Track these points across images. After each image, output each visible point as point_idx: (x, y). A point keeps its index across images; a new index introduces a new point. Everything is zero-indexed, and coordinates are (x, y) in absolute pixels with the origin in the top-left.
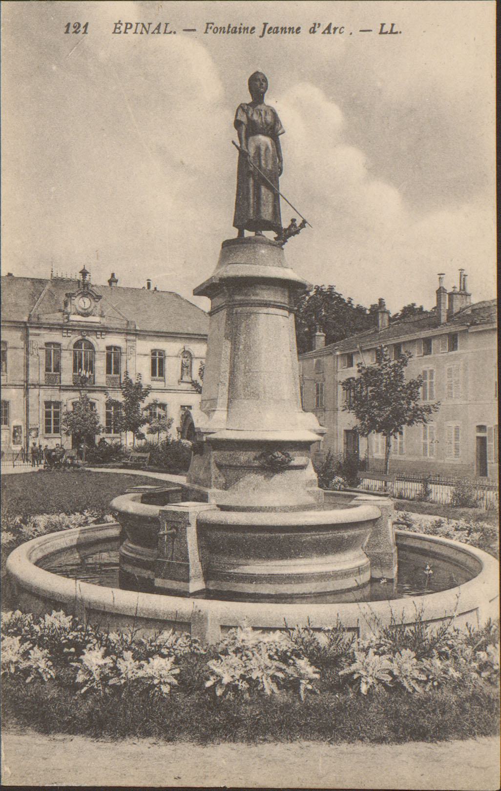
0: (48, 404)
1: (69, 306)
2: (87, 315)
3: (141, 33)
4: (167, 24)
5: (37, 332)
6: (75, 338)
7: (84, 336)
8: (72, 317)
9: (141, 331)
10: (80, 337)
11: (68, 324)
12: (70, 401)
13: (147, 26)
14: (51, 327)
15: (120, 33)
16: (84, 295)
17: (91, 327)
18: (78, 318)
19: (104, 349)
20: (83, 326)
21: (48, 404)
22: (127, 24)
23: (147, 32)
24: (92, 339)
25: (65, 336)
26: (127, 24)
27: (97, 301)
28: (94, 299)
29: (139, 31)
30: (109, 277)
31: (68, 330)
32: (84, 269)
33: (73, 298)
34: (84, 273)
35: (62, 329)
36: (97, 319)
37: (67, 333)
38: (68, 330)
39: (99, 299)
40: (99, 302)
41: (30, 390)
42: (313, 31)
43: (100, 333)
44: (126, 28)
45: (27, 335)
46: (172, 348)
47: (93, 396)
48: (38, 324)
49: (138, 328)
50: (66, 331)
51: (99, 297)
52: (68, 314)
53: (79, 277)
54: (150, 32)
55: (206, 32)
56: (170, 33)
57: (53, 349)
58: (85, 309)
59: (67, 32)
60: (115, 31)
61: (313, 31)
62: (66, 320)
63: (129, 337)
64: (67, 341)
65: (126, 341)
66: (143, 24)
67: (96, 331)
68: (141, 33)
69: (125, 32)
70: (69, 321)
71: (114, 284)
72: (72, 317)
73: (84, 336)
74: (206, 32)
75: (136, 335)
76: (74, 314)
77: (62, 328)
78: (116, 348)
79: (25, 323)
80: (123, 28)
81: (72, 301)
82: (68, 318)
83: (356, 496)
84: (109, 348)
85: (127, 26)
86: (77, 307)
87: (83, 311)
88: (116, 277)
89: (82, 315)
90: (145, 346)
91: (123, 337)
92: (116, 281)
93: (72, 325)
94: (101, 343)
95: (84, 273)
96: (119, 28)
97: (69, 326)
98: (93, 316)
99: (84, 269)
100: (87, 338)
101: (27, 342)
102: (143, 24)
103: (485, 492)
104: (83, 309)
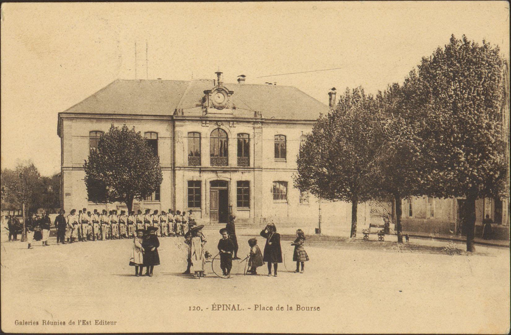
0: (191, 183)
1: (207, 102)
3: (226, 310)
4: (238, 305)
5: (181, 123)
6: (213, 126)
7: (220, 126)
9: (265, 119)
11: (206, 116)
13: (229, 306)
14: (193, 120)
15: (216, 310)
18: (214, 110)
21: (191, 183)
23: (229, 309)
25: (204, 126)
26: (218, 305)
27: (230, 96)
28: (227, 94)
29: (225, 309)
31: (206, 121)
33: (210, 94)
35: (202, 121)
36: (230, 111)
37: (206, 123)
38: (206, 121)
39: (231, 94)
40: (231, 97)
41: (176, 171)
43: (232, 123)
44: (218, 308)
45: (174, 127)
48: (183, 117)
49: (263, 117)
50: (204, 122)
51: (231, 93)
53: (215, 77)
54: (231, 309)
55: (255, 310)
56: (241, 310)
57: (195, 136)
58: (220, 104)
59: (190, 310)
63: (256, 126)
64: (206, 130)
65: (254, 128)
67: (229, 121)
68: (226, 310)
69: (218, 310)
73: (220, 126)
74: (255, 310)
75: (262, 123)
76: (211, 108)
77: (203, 120)
79: (172, 116)
80: (217, 308)
81: (209, 97)
82: (206, 111)
89: (218, 108)
91: (251, 125)
96: (215, 307)
97: (207, 117)
98: (227, 108)
100: (222, 127)
101: (174, 133)
102: (226, 305)
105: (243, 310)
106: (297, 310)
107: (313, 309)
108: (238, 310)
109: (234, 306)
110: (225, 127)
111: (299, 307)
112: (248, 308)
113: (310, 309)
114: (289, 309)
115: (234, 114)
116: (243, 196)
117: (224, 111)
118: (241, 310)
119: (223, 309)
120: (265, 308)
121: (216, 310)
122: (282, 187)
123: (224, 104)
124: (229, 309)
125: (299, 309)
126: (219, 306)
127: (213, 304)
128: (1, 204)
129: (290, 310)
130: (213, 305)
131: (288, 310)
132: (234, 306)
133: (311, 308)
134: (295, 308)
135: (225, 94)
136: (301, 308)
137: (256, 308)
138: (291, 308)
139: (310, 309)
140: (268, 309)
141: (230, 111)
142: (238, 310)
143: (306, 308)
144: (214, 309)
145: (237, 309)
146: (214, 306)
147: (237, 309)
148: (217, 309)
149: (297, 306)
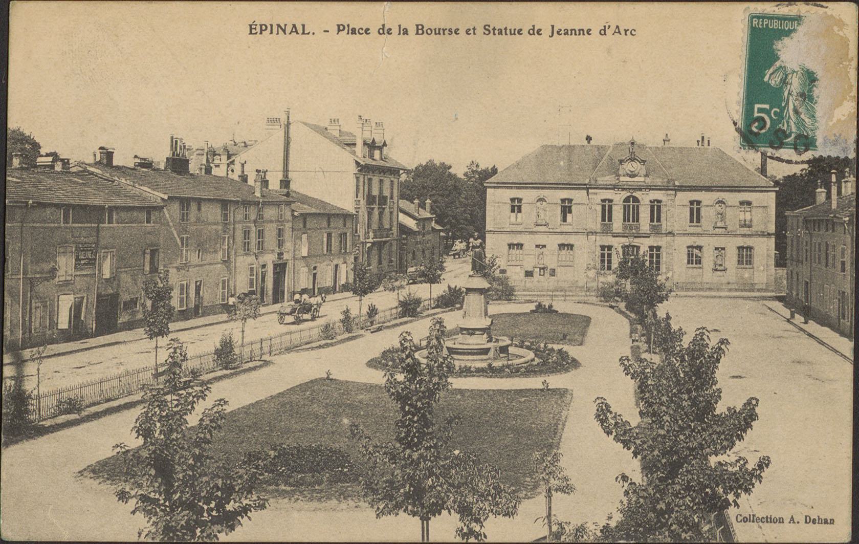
2: (634, 176)
6: (625, 194)
8: (622, 179)
10: (629, 194)
16: (632, 160)
18: (628, 179)
22: (261, 26)
24: (637, 194)
26: (261, 26)
36: (642, 179)
38: (618, 189)
42: (603, 32)
46: (706, 198)
47: (636, 242)
56: (308, 34)
58: (632, 172)
61: (603, 32)
66: (285, 34)
76: (624, 176)
80: (258, 30)
82: (618, 179)
89: (630, 176)
90: (685, 197)
92: (669, 141)
94: (645, 198)
96: (255, 29)
100: (634, 194)
105: (313, 34)
106: (417, 33)
107: (447, 32)
108: (303, 33)
109: (294, 26)
110: (637, 194)
111: (422, 29)
112: (328, 31)
113: (441, 32)
114: (402, 32)
115: (646, 181)
116: (607, 206)
117: (636, 179)
118: (308, 34)
119: (270, 32)
121: (256, 33)
122: (696, 251)
123: (636, 172)
124: (284, 31)
125: (420, 32)
126: (264, 27)
127: (251, 23)
128: (596, 542)
129: (404, 34)
130: (251, 26)
131: (399, 34)
132: (294, 26)
133: (444, 30)
134: (412, 30)
135: (638, 163)
137: (615, 32)
138: (406, 32)
139: (441, 32)
140: (361, 31)
141: (642, 179)
142: (303, 33)
143: (434, 31)
144: (254, 31)
145: (300, 31)
146: (253, 27)
147: (300, 31)
148: (259, 32)
149: (417, 28)
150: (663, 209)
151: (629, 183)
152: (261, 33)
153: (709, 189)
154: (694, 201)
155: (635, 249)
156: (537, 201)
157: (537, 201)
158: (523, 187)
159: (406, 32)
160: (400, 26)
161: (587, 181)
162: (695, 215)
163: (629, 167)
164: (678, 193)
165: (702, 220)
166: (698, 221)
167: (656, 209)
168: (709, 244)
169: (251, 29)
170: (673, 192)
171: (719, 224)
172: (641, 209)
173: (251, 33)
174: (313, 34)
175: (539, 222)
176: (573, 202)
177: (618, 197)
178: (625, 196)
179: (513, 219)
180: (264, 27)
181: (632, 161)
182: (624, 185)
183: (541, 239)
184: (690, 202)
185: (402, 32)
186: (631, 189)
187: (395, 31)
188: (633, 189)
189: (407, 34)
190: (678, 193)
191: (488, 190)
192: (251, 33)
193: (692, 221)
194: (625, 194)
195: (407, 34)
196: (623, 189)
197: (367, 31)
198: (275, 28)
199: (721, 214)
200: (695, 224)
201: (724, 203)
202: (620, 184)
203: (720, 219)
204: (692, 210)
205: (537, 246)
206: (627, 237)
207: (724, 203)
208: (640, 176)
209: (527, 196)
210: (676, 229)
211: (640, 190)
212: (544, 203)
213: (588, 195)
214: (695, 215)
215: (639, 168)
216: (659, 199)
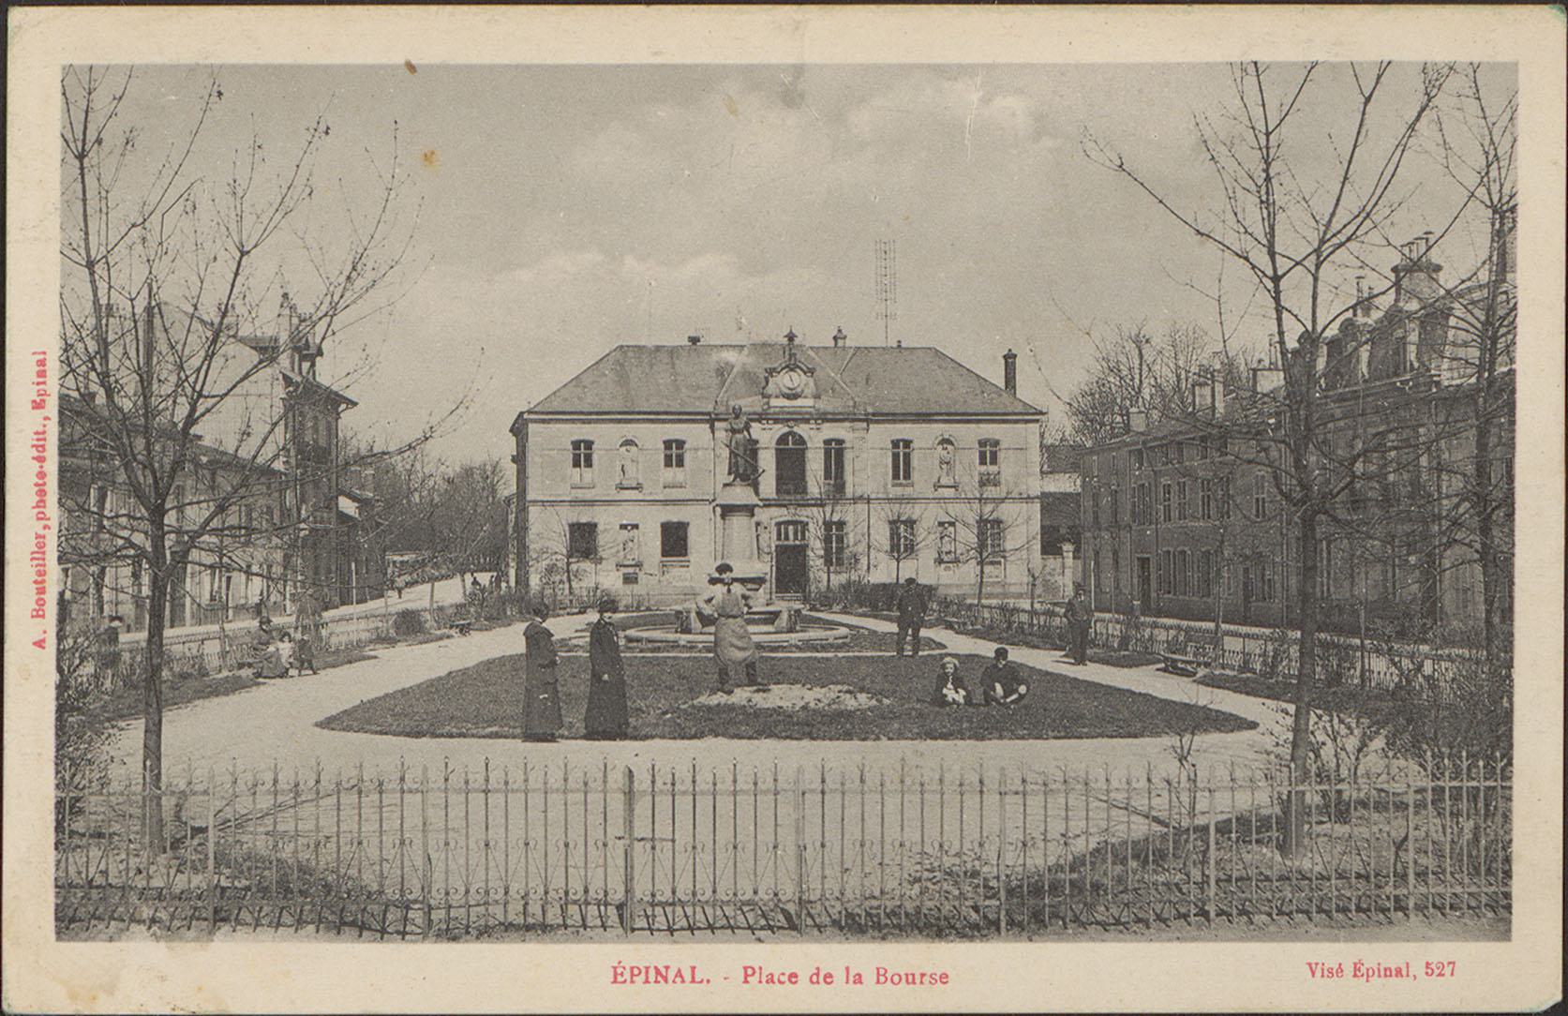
2: (795, 397)
6: (781, 429)
8: (774, 402)
10: (786, 430)
12: (773, 522)
13: (663, 971)
16: (791, 368)
17: (799, 413)
19: (822, 445)
20: (789, 413)
22: (632, 968)
23: (666, 981)
24: (802, 430)
26: (632, 968)
28: (805, 373)
29: (652, 979)
30: (835, 333)
32: (791, 332)
34: (791, 337)
36: (810, 402)
44: (632, 975)
46: (922, 435)
47: (803, 514)
52: (769, 397)
54: (670, 979)
56: (701, 982)
60: (615, 978)
62: (766, 407)
66: (656, 968)
68: (656, 982)
69: (632, 982)
70: (769, 408)
71: (840, 343)
72: (774, 402)
76: (777, 397)
78: (840, 442)
80: (627, 975)
82: (768, 403)
83: (1065, 656)
84: (827, 442)
85: (632, 971)
86: (781, 386)
87: (789, 392)
88: (844, 332)
89: (788, 397)
90: (882, 435)
93: (774, 413)
94: (816, 437)
95: (791, 337)
96: (622, 974)
99: (791, 332)
100: (795, 429)
103: (1187, 738)
104: (789, 389)
106: (878, 982)
108: (693, 981)
110: (802, 430)
114: (851, 979)
117: (799, 402)
118: (701, 982)
120: (904, 980)
121: (625, 981)
123: (799, 390)
127: (616, 964)
129: (855, 982)
136: (889, 975)
137: (746, 975)
138: (859, 979)
142: (693, 981)
144: (620, 979)
146: (619, 971)
148: (629, 980)
150: (848, 456)
151: (786, 409)
152: (632, 982)
153: (924, 417)
154: (898, 441)
155: (791, 528)
156: (621, 446)
157: (621, 446)
158: (603, 420)
159: (859, 979)
160: (847, 969)
161: (710, 408)
162: (902, 465)
163: (786, 380)
164: (871, 426)
165: (915, 475)
166: (907, 476)
167: (835, 452)
168: (928, 516)
169: (616, 974)
170: (865, 425)
171: (944, 481)
172: (809, 454)
173: (615, 981)
174: (708, 981)
175: (626, 483)
176: (686, 446)
177: (766, 436)
178: (780, 433)
179: (576, 478)
180: (636, 972)
181: (792, 370)
182: (778, 414)
183: (629, 514)
184: (893, 442)
185: (851, 979)
186: (788, 420)
187: (839, 976)
188: (793, 420)
189: (861, 983)
190: (871, 426)
191: (530, 425)
192: (615, 981)
193: (896, 476)
194: (781, 429)
195: (861, 983)
196: (776, 421)
197: (793, 977)
198: (652, 974)
199: (947, 463)
200: (902, 480)
201: (952, 444)
202: (772, 410)
203: (945, 471)
204: (896, 456)
205: (623, 527)
206: (785, 506)
207: (952, 444)
208: (805, 397)
209: (605, 436)
210: (869, 489)
211: (807, 421)
212: (634, 449)
213: (713, 432)
214: (902, 465)
215: (804, 382)
216: (841, 437)
